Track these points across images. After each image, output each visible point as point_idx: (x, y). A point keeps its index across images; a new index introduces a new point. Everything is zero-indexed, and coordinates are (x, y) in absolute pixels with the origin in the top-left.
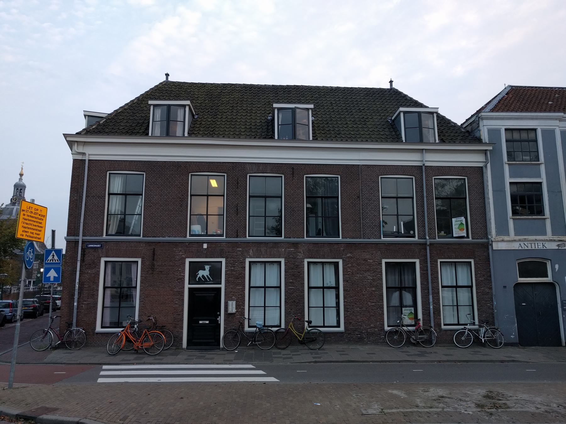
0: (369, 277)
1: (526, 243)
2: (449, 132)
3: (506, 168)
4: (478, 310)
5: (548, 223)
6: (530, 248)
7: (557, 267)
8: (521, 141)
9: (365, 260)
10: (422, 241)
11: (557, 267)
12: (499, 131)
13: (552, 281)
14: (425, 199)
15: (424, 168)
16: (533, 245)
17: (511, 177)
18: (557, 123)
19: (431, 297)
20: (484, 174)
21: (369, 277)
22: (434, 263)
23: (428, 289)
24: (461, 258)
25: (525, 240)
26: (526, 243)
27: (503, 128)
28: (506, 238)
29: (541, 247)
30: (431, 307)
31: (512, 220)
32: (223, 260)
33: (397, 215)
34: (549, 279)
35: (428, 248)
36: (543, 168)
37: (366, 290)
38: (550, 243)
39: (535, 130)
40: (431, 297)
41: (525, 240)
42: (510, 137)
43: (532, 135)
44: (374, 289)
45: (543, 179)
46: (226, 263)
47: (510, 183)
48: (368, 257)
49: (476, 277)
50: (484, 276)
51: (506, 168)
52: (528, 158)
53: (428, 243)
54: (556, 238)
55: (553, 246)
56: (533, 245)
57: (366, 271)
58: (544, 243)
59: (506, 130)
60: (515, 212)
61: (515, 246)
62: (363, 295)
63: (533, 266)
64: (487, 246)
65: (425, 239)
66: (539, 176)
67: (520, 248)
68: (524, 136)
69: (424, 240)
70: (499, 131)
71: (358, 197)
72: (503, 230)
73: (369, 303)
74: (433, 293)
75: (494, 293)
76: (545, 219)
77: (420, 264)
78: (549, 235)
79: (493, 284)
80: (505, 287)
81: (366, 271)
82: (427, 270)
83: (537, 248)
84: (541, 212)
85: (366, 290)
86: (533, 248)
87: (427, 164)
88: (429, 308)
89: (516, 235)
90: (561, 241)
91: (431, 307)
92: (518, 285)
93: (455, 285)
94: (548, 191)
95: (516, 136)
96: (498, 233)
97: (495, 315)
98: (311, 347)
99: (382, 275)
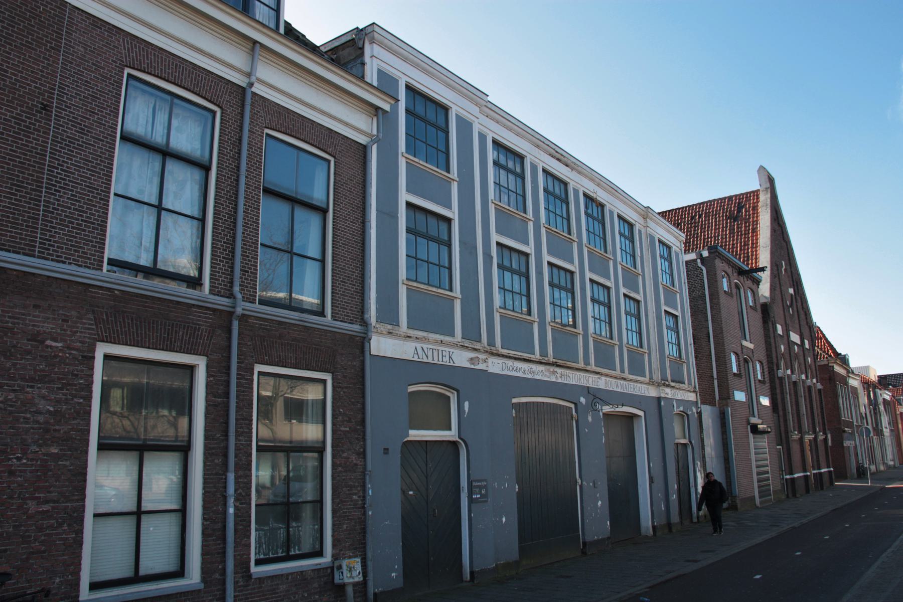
0: (42, 405)
2: (609, 538)
4: (334, 512)
6: (430, 360)
7: (467, 404)
9: (37, 338)
10: (222, 302)
14: (243, 180)
15: (249, 97)
19: (231, 477)
20: (368, 163)
21: (42, 405)
22: (246, 372)
23: (226, 456)
30: (231, 510)
31: (405, 287)
33: (159, 208)
35: (235, 324)
37: (24, 452)
40: (231, 477)
44: (54, 450)
48: (48, 327)
50: (349, 421)
53: (239, 311)
57: (32, 379)
62: (12, 473)
64: (361, 343)
65: (231, 296)
67: (416, 359)
69: (225, 301)
71: (45, 107)
73: (32, 506)
74: (237, 467)
75: (369, 467)
77: (209, 374)
81: (32, 379)
82: (227, 395)
85: (24, 452)
87: (258, 89)
88: (225, 512)
91: (231, 510)
93: (143, 509)
97: (370, 522)
99: (89, 398)
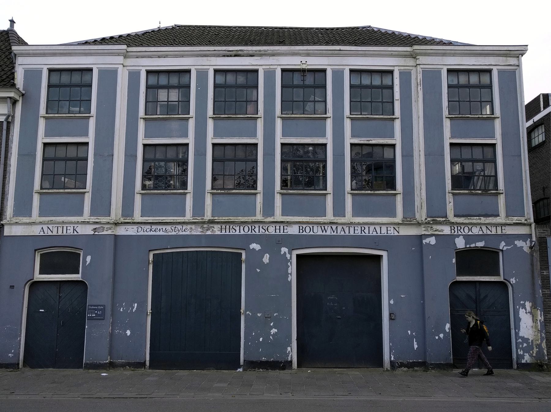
1: (50, 226)
3: (42, 123)
5: (88, 199)
6: (55, 233)
7: (89, 259)
8: (70, 86)
11: (89, 259)
12: (438, 72)
13: (81, 279)
16: (60, 230)
17: (284, 135)
18: (120, 59)
25: (51, 222)
26: (50, 226)
27: (445, 69)
28: (26, 220)
29: (70, 232)
31: (350, 196)
34: (500, 279)
36: (92, 123)
38: (83, 226)
39: (324, 71)
41: (51, 222)
42: (356, 82)
43: (485, 79)
45: (498, 140)
47: (452, 145)
51: (42, 123)
52: (77, 109)
54: (93, 219)
55: (88, 230)
56: (60, 230)
58: (76, 226)
59: (352, 71)
60: (284, 184)
61: (36, 231)
63: (61, 258)
66: (392, 136)
67: (42, 234)
70: (39, 72)
72: (24, 208)
76: (325, 195)
78: (86, 215)
80: (12, 287)
83: (65, 233)
84: (392, 185)
86: (60, 233)
90: (97, 223)
92: (35, 285)
94: (95, 155)
95: (366, 80)
96: (18, 212)
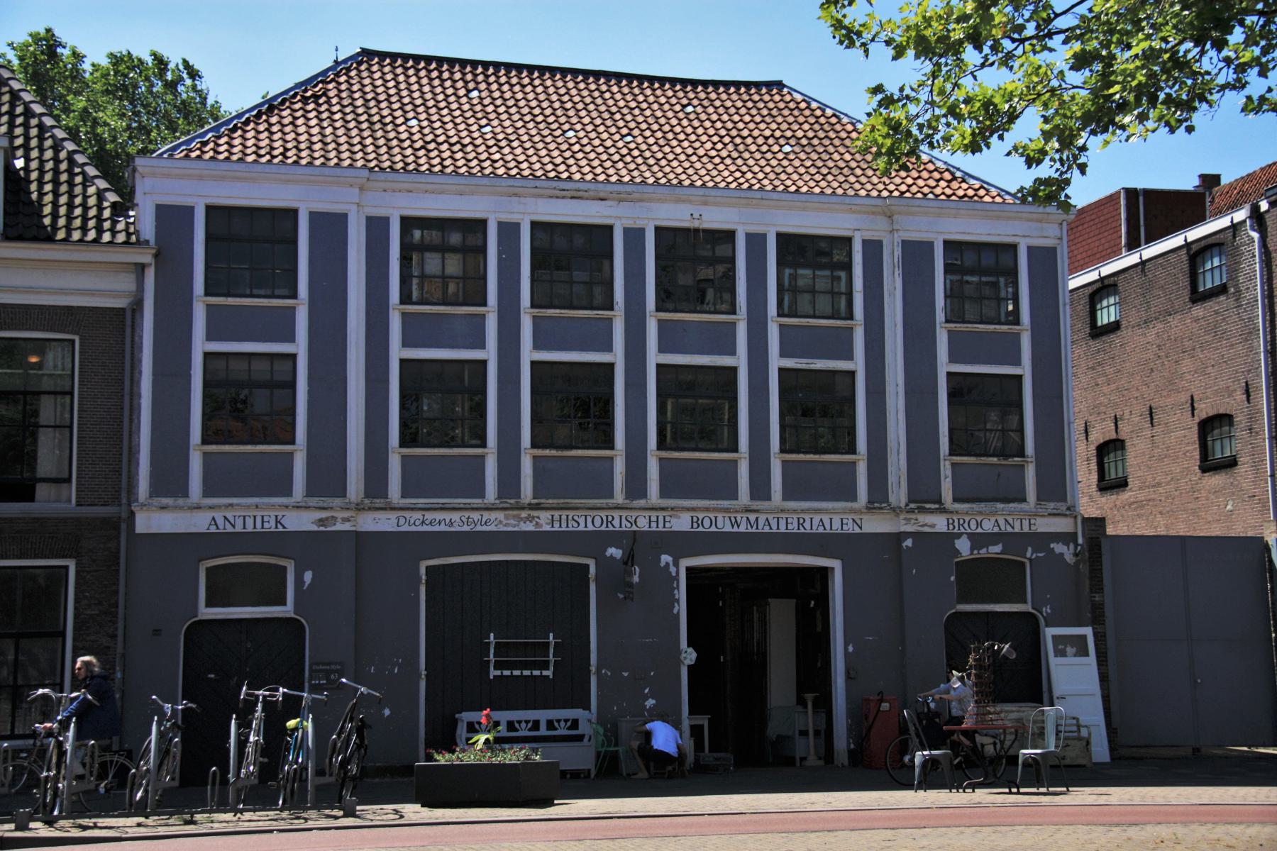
1: (1010, 519)
6: (1017, 529)
7: (308, 576)
11: (308, 576)
24: (36, 557)
32: (72, 565)
43: (1005, 259)
46: (78, 573)
47: (949, 374)
49: (76, 608)
50: (100, 603)
68: (988, 260)
72: (170, 482)
79: (120, 625)
80: (157, 632)
83: (259, 529)
86: (250, 528)
89: (785, 498)
95: (969, 259)
98: (327, 812)
